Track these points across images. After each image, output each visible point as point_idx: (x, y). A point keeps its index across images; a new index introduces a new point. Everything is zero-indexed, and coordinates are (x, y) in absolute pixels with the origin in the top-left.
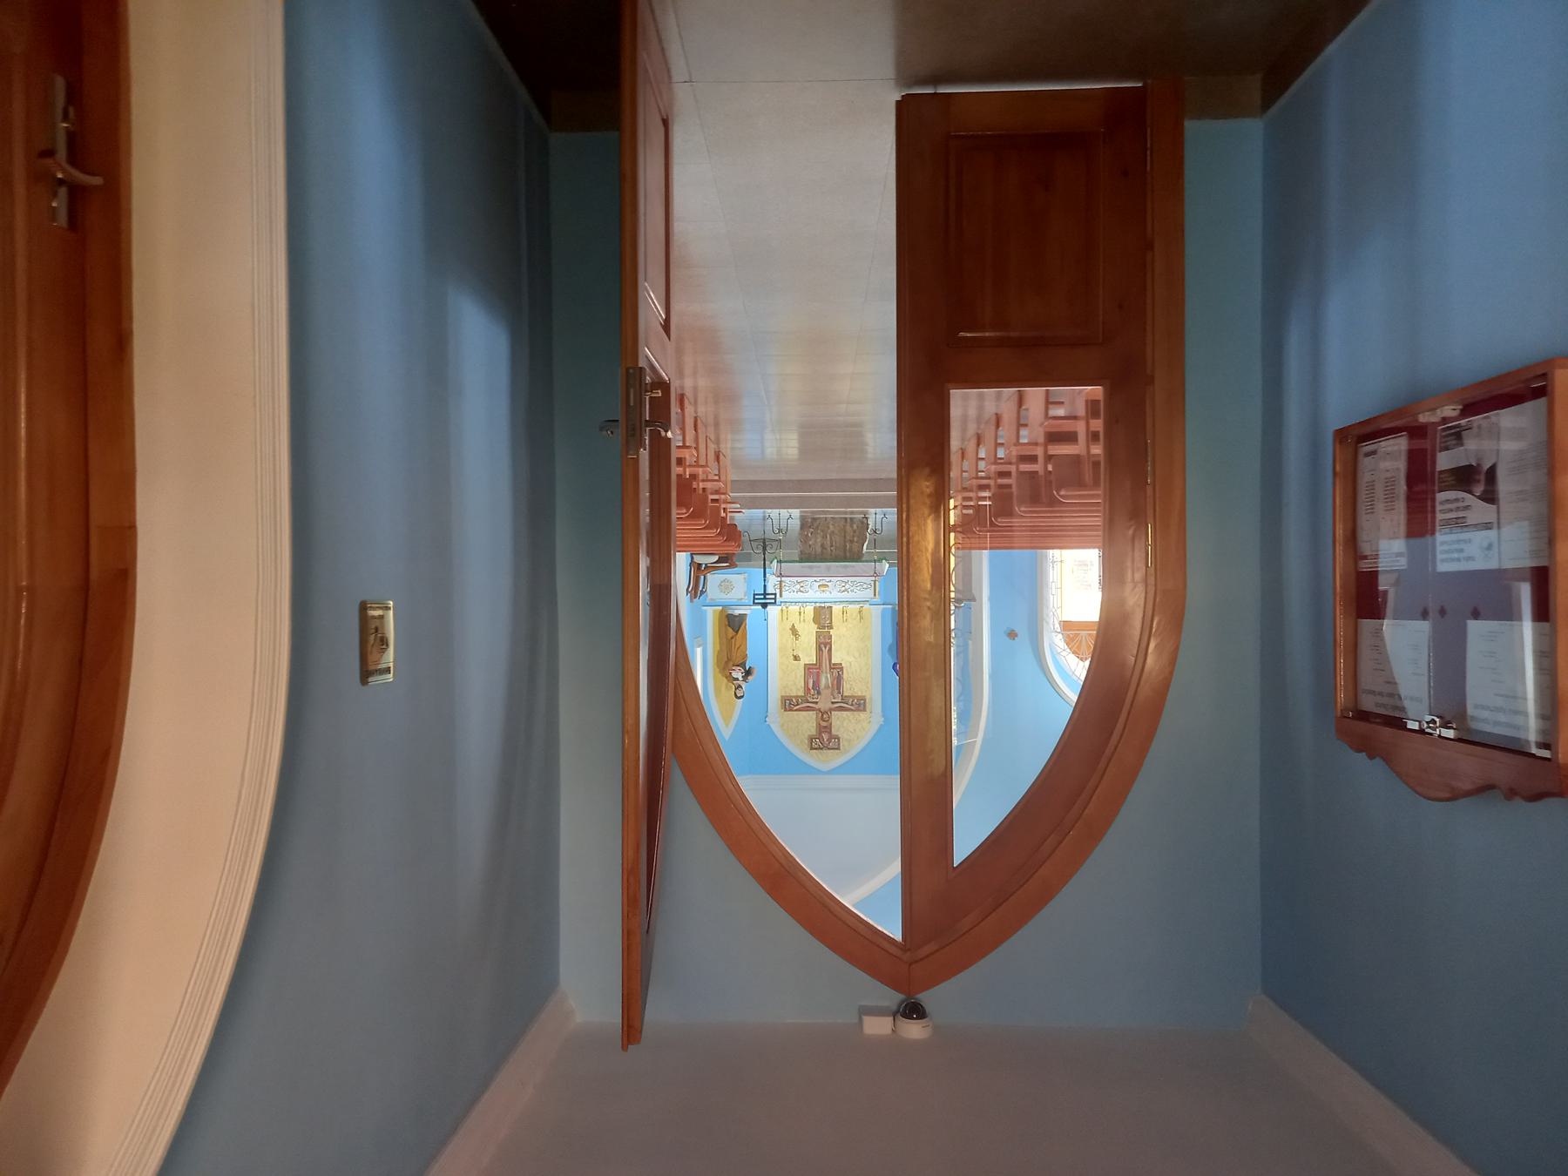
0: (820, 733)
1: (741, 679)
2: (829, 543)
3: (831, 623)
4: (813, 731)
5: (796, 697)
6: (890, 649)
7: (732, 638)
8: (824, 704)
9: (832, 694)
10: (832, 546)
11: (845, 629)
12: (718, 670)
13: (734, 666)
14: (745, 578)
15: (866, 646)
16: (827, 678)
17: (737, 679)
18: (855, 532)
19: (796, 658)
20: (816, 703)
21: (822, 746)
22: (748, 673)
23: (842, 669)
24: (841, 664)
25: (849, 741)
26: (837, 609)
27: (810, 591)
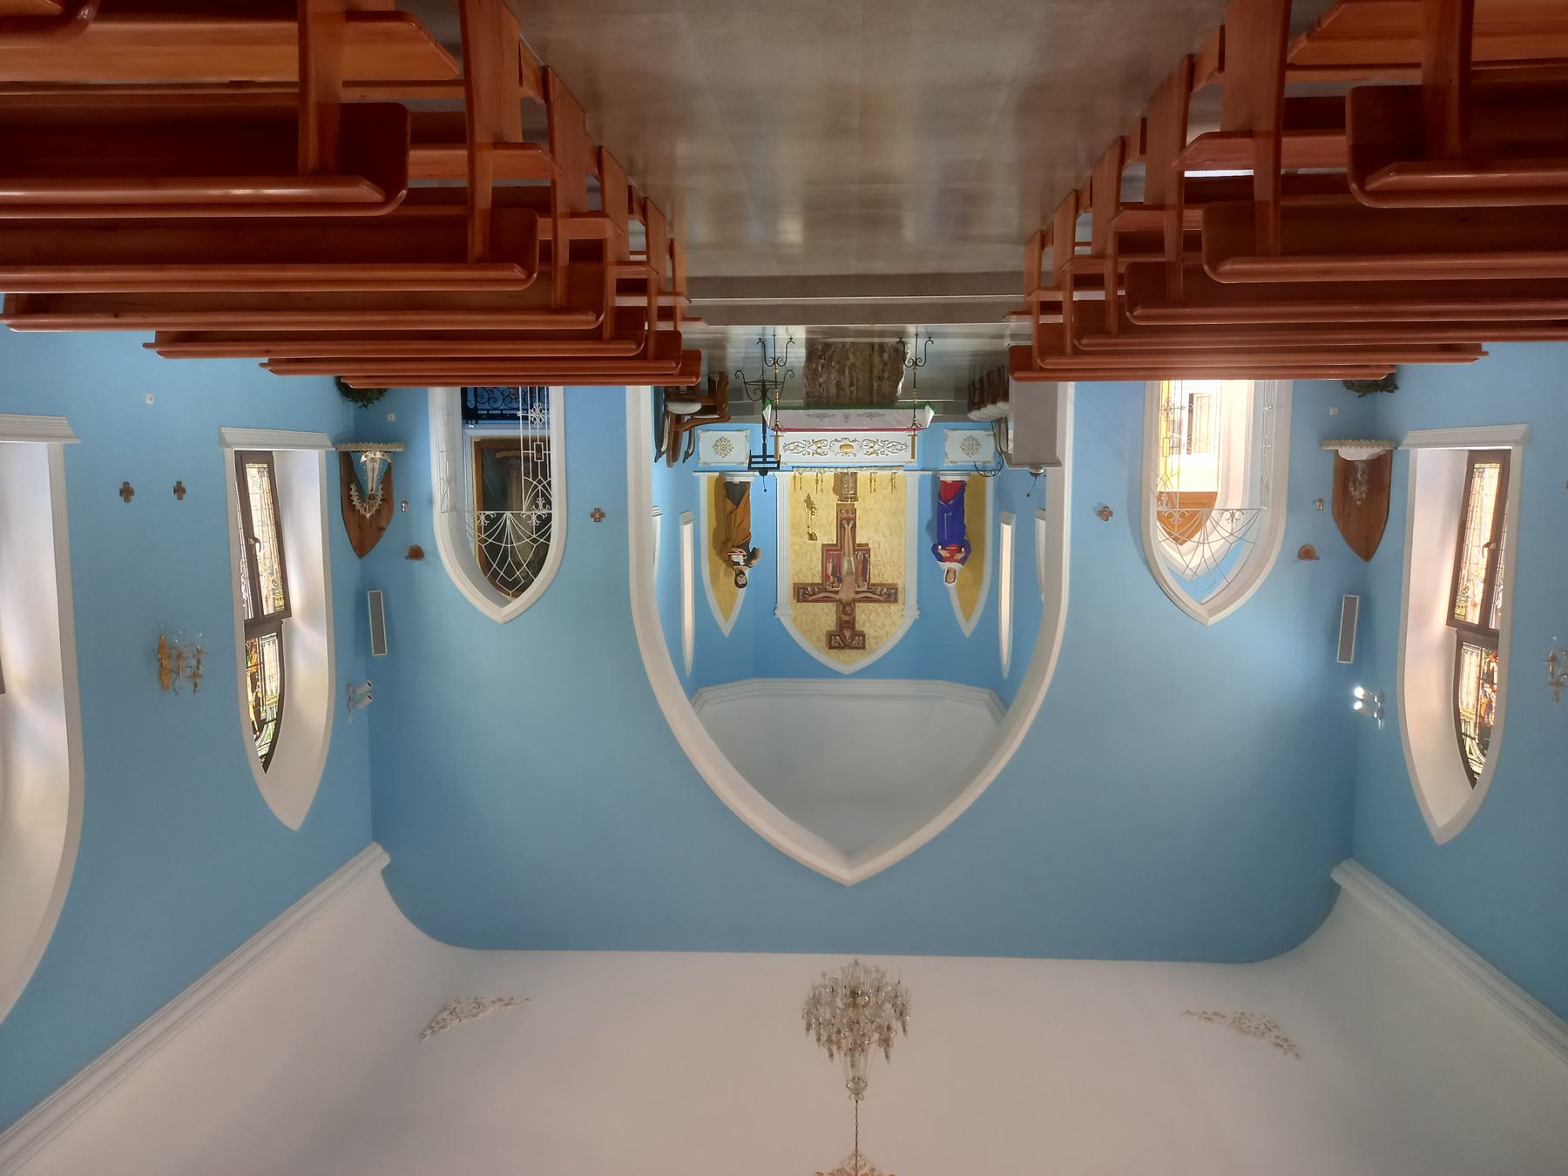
1: (742, 563)
2: (847, 380)
5: (813, 585)
7: (731, 512)
8: (846, 594)
9: (856, 582)
10: (852, 385)
13: (733, 547)
14: (746, 437)
15: (899, 522)
16: (849, 561)
17: (738, 564)
19: (812, 537)
20: (837, 592)
22: (751, 556)
23: (868, 551)
26: (863, 476)
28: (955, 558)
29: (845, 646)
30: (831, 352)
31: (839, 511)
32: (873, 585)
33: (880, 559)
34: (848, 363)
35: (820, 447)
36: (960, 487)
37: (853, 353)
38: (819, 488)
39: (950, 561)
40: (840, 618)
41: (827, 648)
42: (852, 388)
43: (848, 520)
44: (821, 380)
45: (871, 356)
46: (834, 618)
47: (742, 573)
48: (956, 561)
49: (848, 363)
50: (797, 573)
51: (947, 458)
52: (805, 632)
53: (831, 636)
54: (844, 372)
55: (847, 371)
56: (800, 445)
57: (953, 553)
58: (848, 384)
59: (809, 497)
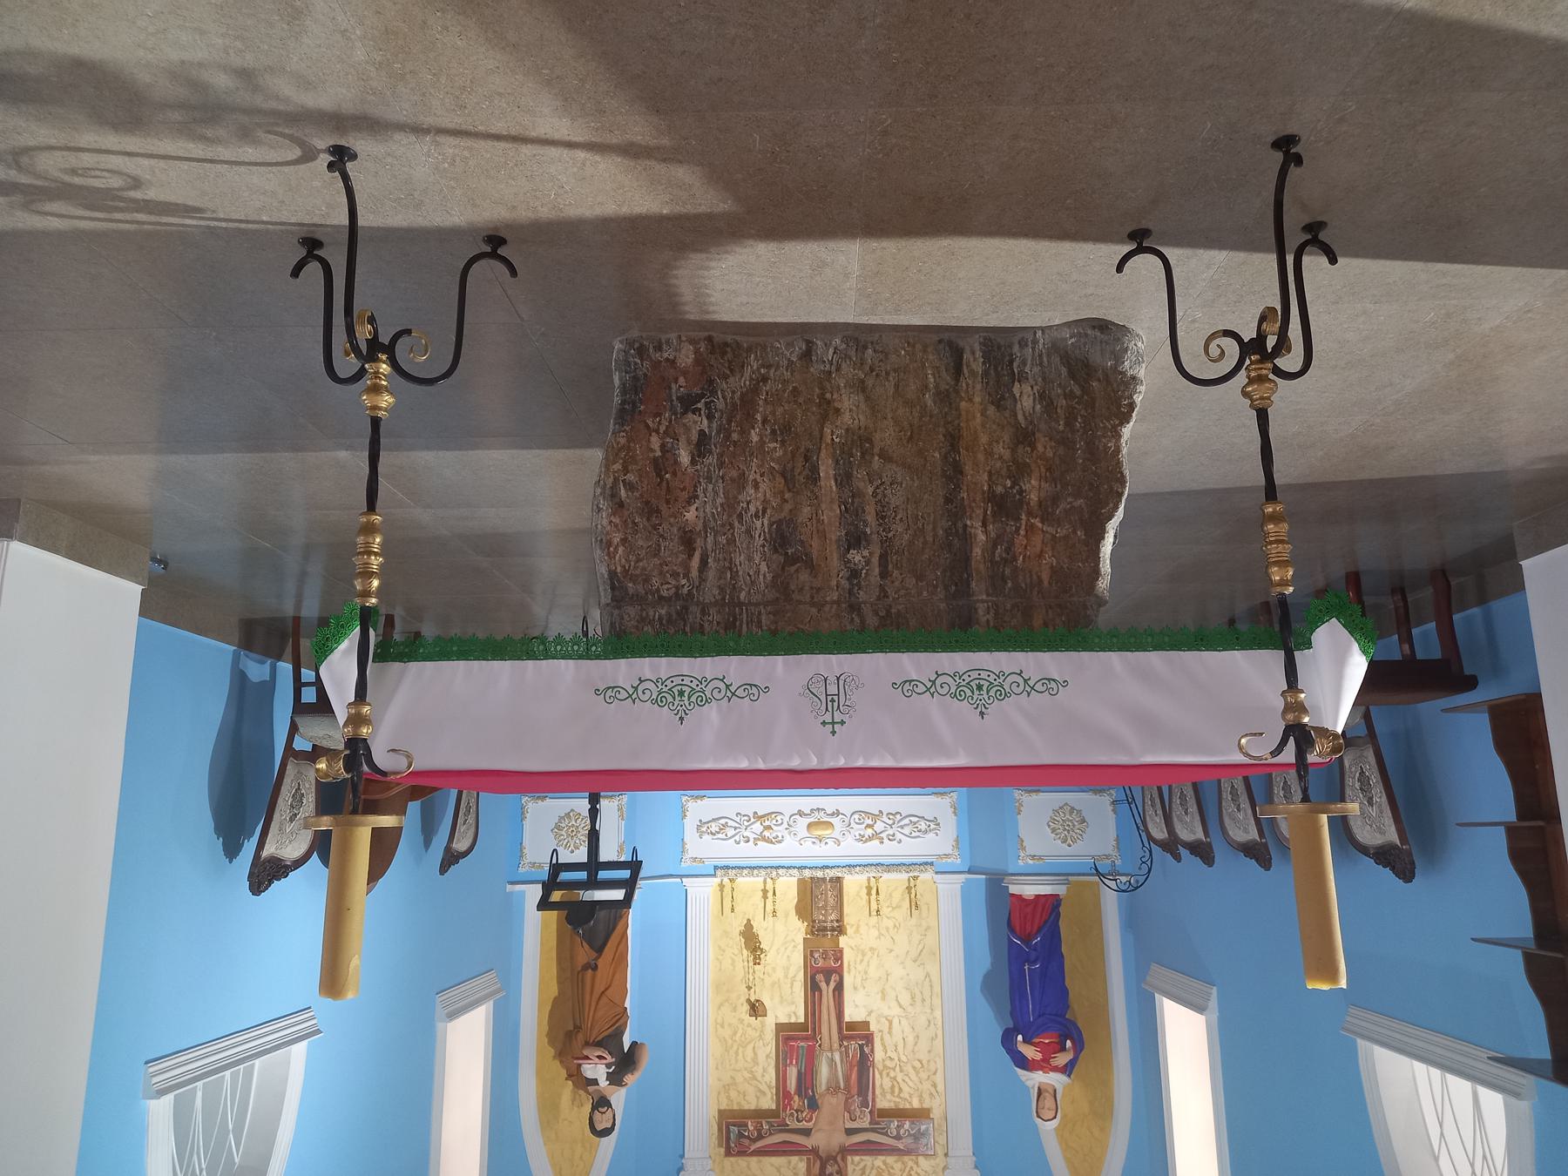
1: (603, 1083)
2: (830, 514)
5: (759, 1114)
6: (988, 984)
7: (586, 967)
8: (826, 1136)
9: (847, 1109)
10: (855, 540)
12: (551, 1052)
13: (587, 1044)
14: (620, 809)
15: (928, 975)
16: (832, 1061)
17: (595, 1082)
18: (1024, 437)
19: (756, 1009)
20: (807, 1132)
22: (626, 1062)
23: (869, 1039)
24: (866, 1024)
26: (853, 884)
27: (788, 839)
28: (1055, 1062)
30: (739, 383)
31: (809, 954)
33: (894, 1055)
34: (833, 433)
35: (769, 828)
36: (1049, 907)
37: (861, 387)
38: (769, 907)
39: (1042, 1068)
42: (856, 557)
43: (828, 973)
44: (691, 515)
45: (946, 398)
47: (602, 1103)
48: (1056, 1069)
49: (833, 433)
50: (727, 1088)
54: (814, 477)
55: (826, 469)
56: (731, 823)
57: (1048, 1052)
58: (836, 533)
59: (749, 926)
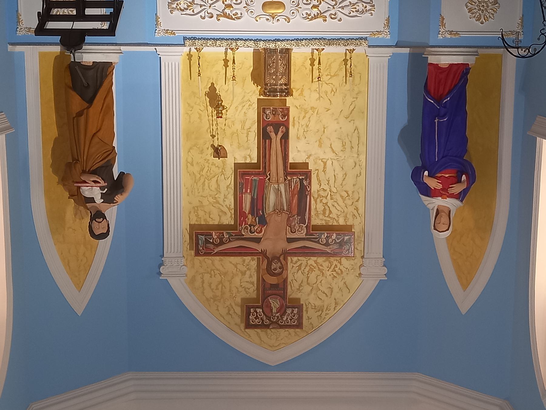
0: (265, 297)
1: (99, 200)
3: (288, 84)
4: (252, 292)
5: (221, 227)
7: (80, 114)
9: (289, 224)
11: (315, 95)
12: (56, 179)
13: (84, 172)
15: (356, 129)
16: (278, 190)
17: (92, 200)
19: (219, 152)
20: (258, 240)
21: (267, 322)
23: (308, 175)
24: (306, 164)
25: (320, 309)
28: (451, 191)
29: (272, 323)
32: (317, 228)
33: (326, 187)
39: (441, 195)
40: (263, 280)
41: (243, 326)
43: (277, 126)
46: (255, 279)
47: (98, 215)
48: (452, 196)
50: (196, 209)
51: (444, 25)
52: (207, 300)
53: (248, 308)
59: (213, 88)
